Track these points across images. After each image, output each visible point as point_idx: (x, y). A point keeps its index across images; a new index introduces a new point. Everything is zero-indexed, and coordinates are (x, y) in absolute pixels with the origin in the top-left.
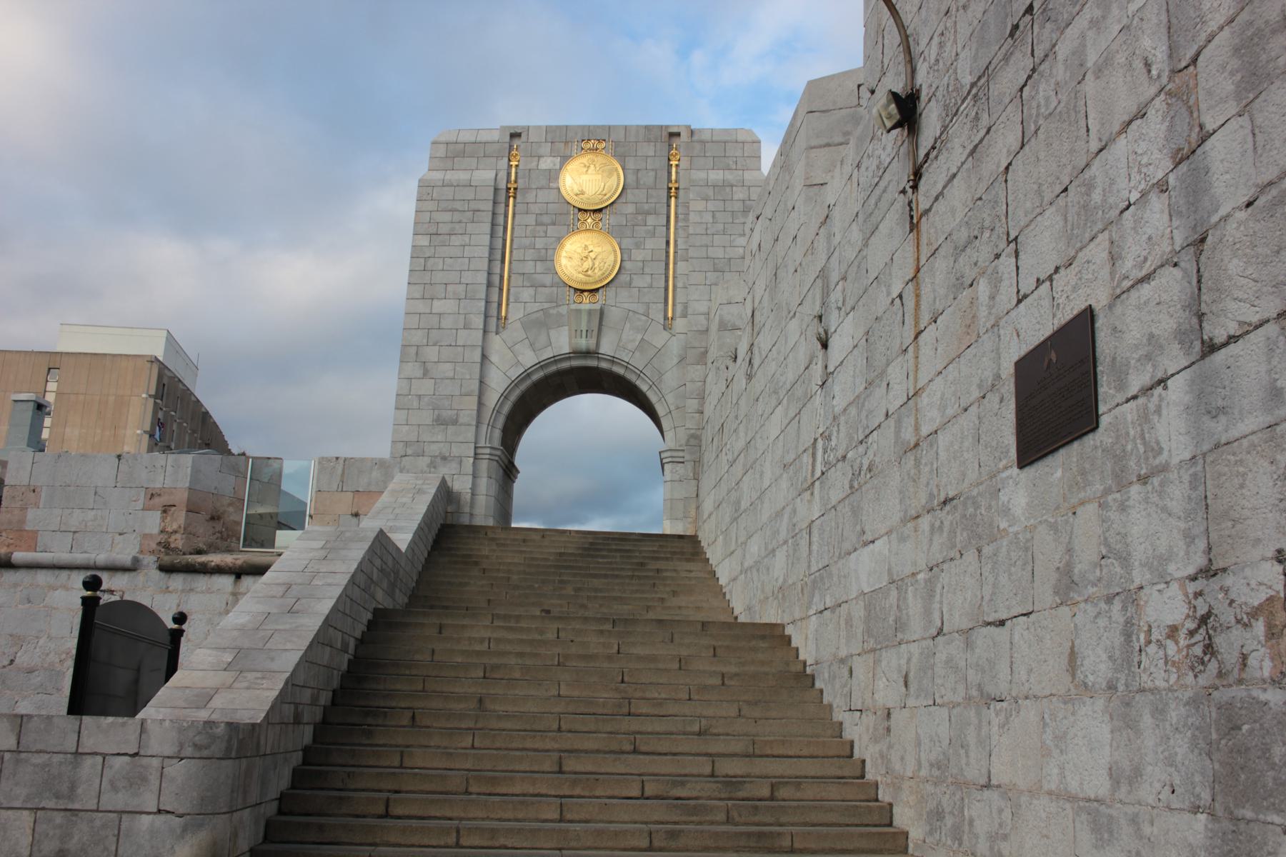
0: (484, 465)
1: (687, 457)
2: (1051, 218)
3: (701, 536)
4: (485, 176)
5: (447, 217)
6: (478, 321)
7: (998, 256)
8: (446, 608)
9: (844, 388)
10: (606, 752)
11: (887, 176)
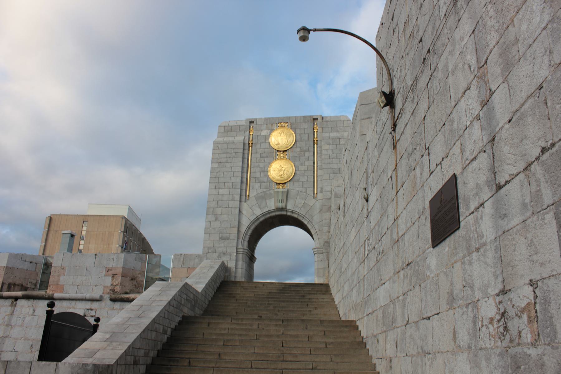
0: (240, 256)
1: (324, 251)
2: (440, 137)
5: (225, 155)
6: (237, 197)
7: (422, 156)
8: (219, 315)
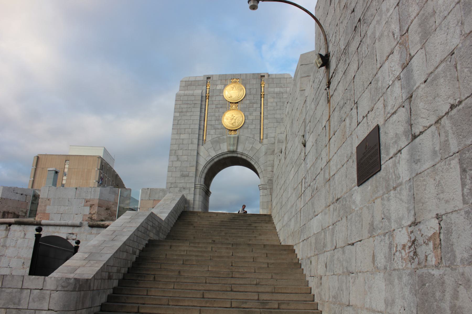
0: (198, 191)
1: (268, 187)
2: (367, 94)
3: (272, 215)
4: (198, 92)
5: (186, 106)
6: (196, 141)
7: (352, 109)
8: (179, 240)
9: (310, 159)
10: (221, 291)
11: (321, 85)
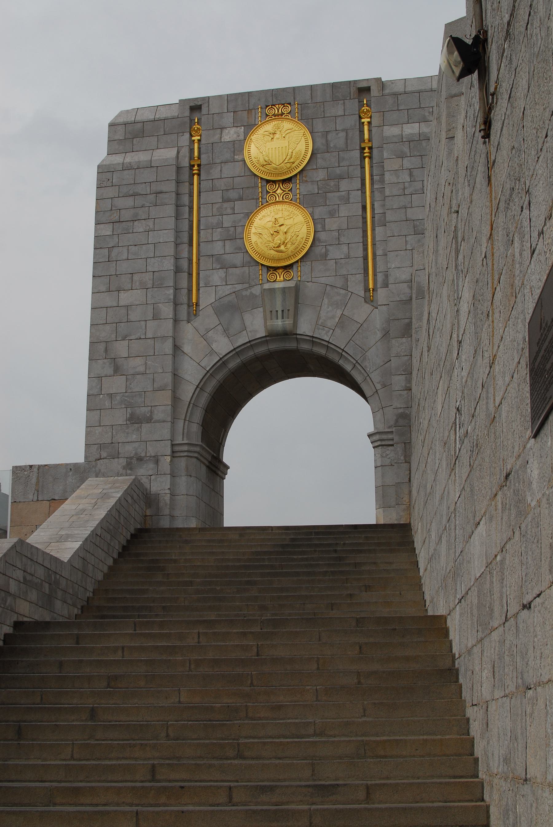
1: (396, 438)
5: (129, 202)
6: (167, 310)
